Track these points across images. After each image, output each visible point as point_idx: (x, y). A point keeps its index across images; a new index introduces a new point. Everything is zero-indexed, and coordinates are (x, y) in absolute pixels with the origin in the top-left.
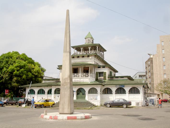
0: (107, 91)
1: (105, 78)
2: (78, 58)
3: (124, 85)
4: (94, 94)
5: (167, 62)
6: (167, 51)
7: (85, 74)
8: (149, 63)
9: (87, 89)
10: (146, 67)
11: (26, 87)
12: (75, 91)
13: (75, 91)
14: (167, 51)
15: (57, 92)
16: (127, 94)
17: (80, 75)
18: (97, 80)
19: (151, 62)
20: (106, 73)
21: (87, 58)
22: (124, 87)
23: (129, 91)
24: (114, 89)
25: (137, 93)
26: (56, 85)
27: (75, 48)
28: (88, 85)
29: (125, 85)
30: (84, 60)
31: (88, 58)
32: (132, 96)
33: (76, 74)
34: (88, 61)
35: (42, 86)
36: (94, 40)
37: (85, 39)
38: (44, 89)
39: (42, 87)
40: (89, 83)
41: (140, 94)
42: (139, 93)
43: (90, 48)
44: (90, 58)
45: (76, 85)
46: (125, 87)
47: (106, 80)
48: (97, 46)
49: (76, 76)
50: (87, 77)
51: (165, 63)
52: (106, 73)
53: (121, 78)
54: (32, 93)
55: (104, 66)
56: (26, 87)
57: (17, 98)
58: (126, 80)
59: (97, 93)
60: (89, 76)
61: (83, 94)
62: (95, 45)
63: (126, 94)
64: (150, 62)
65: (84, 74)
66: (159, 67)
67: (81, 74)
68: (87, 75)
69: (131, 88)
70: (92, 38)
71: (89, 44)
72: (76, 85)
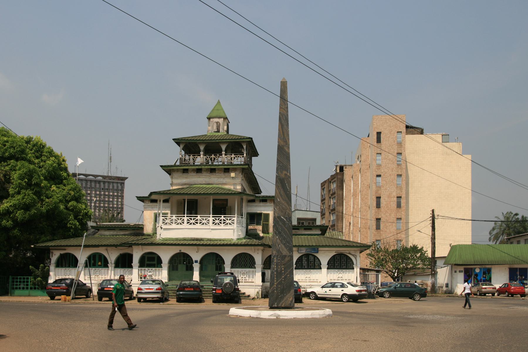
0: (308, 260)
1: (265, 230)
2: (199, 174)
3: (316, 248)
4: (237, 268)
5: (386, 189)
6: (389, 160)
7: (224, 218)
8: (334, 186)
9: (228, 257)
10: (322, 196)
11: (50, 248)
12: (196, 262)
13: (196, 262)
14: (389, 160)
15: (147, 262)
16: (324, 270)
17: (235, 219)
18: (250, 234)
19: (339, 185)
20: (267, 215)
21: (222, 175)
22: (317, 252)
23: (328, 264)
24: (324, 258)
25: (346, 268)
26: (145, 244)
27: (183, 143)
28: (230, 245)
29: (320, 249)
30: (216, 179)
31: (227, 174)
32: (335, 275)
33: (223, 216)
34: (224, 182)
35: (98, 246)
36: (229, 124)
37: (209, 119)
38: (105, 254)
39: (100, 248)
40: (235, 241)
41: (355, 269)
42: (351, 269)
43: (224, 147)
44: (233, 175)
45: (199, 245)
46: (319, 252)
47: (268, 233)
48: (244, 142)
49: (222, 222)
50: (229, 227)
51: (380, 192)
52: (267, 215)
53: (305, 229)
54: (67, 265)
55: (264, 199)
56: (50, 248)
57: (20, 279)
58: (318, 235)
59: (255, 268)
60: (235, 222)
61: (187, 269)
62: (244, 139)
63: (322, 269)
64: (337, 185)
65: (222, 218)
66: (362, 199)
67: (213, 218)
68: (230, 222)
69: (334, 256)
70: (225, 118)
71: (219, 134)
72: (199, 245)
